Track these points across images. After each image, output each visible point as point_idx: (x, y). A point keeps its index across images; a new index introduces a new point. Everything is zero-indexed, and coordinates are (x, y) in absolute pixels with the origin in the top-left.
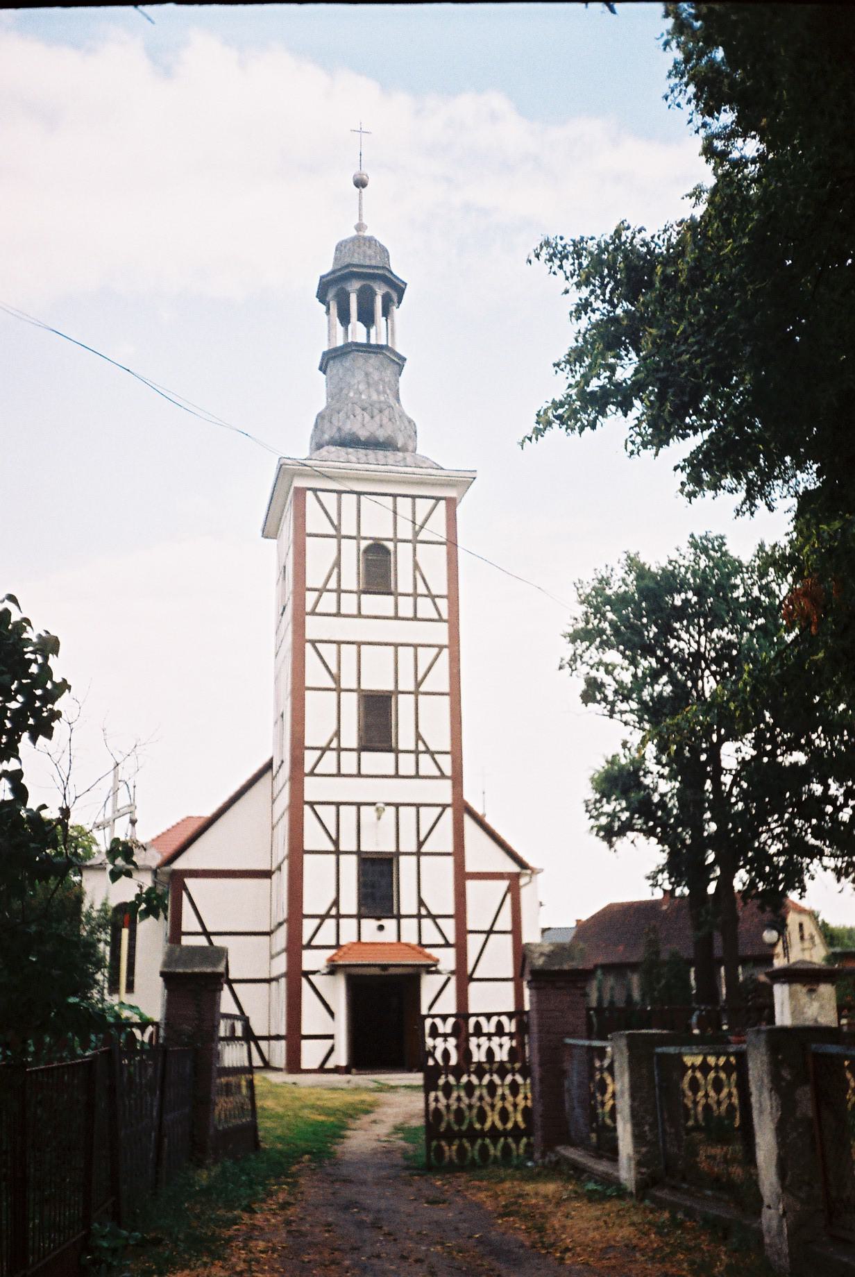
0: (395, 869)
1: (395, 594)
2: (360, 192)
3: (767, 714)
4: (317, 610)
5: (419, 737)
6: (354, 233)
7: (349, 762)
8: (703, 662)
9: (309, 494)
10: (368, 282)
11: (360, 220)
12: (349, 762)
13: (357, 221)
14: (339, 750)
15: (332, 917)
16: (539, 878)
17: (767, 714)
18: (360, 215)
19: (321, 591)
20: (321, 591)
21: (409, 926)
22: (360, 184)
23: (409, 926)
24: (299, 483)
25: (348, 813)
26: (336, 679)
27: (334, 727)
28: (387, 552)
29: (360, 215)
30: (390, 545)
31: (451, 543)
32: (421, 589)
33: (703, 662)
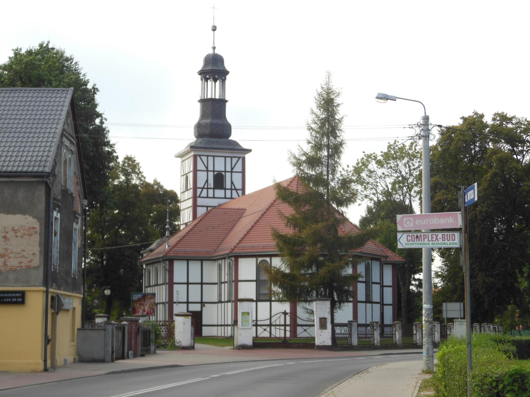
1: (225, 189)
2: (214, 48)
4: (201, 196)
5: (232, 183)
6: (211, 52)
7: (211, 194)
9: (198, 157)
11: (214, 44)
12: (211, 192)
13: (212, 45)
14: (208, 188)
15: (205, 188)
19: (203, 188)
20: (203, 188)
21: (228, 193)
22: (214, 29)
23: (228, 193)
25: (211, 159)
26: (207, 168)
27: (206, 178)
28: (222, 175)
30: (224, 173)
31: (243, 172)
32: (233, 188)
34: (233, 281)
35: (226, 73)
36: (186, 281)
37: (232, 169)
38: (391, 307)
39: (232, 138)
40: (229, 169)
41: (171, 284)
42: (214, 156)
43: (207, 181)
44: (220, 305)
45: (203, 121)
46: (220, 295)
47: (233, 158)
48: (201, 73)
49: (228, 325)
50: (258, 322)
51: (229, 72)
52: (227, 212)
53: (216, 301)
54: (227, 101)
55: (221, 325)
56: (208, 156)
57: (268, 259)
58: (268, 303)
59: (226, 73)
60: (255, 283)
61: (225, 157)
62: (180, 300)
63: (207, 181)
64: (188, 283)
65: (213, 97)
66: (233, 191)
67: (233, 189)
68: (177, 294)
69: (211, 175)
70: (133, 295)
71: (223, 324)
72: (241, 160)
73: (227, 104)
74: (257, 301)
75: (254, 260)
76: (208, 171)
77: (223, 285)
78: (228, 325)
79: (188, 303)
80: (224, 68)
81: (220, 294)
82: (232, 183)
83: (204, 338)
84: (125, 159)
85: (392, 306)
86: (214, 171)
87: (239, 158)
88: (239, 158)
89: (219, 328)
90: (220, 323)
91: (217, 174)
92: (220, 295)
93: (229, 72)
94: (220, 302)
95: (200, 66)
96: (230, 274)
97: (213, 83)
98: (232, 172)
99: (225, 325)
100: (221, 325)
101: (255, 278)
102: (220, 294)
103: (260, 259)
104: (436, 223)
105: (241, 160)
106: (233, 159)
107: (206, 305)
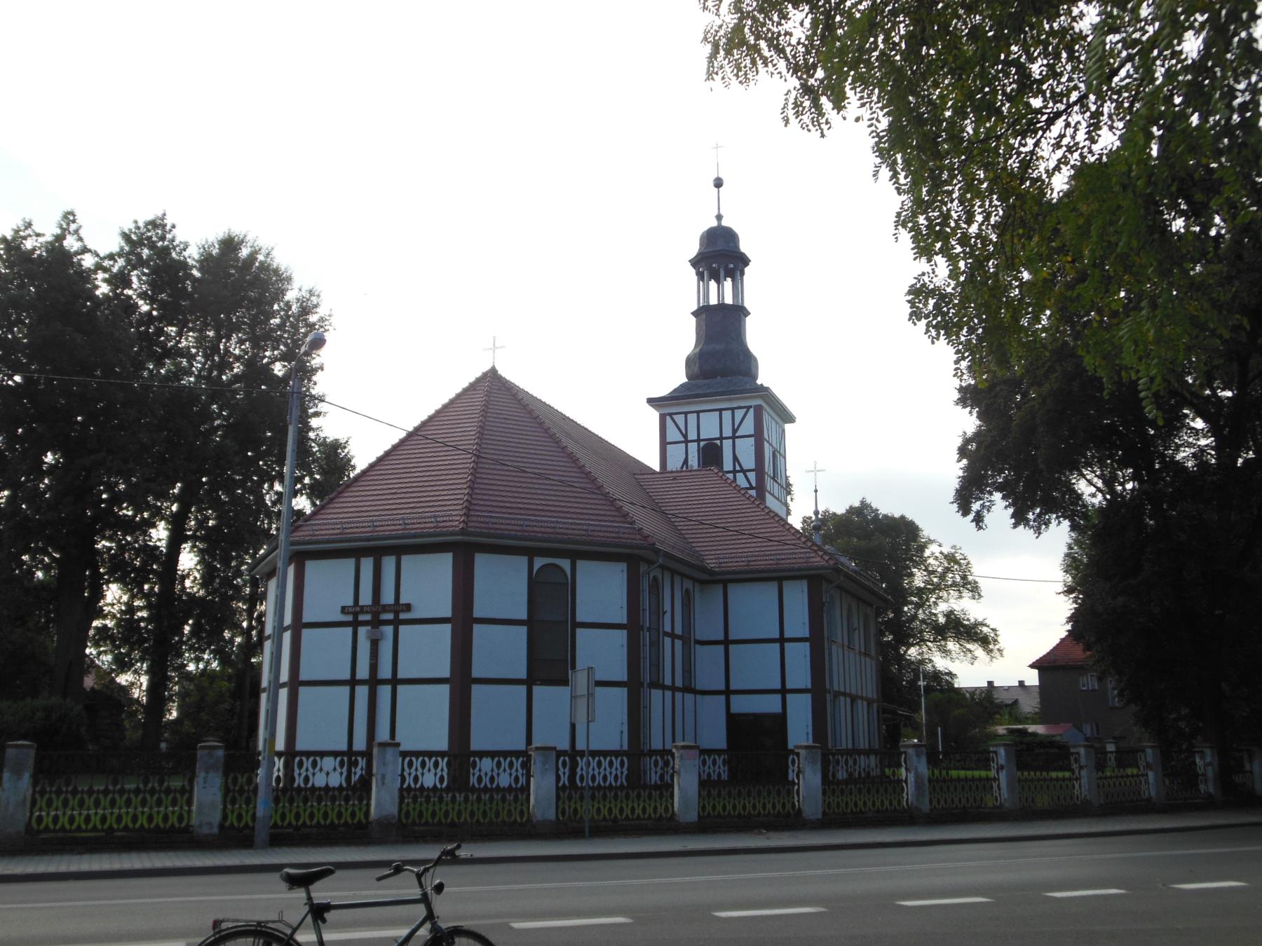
2: (719, 217)
5: (735, 459)
6: (714, 223)
9: (668, 417)
13: (716, 213)
22: (718, 183)
25: (692, 418)
26: (685, 436)
29: (719, 208)
32: (738, 468)
35: (744, 261)
37: (735, 431)
38: (448, 627)
40: (727, 432)
41: (819, 690)
42: (698, 412)
43: (686, 461)
48: (695, 263)
56: (686, 413)
57: (565, 564)
59: (744, 261)
60: (523, 630)
61: (720, 410)
63: (686, 461)
66: (737, 474)
67: (738, 471)
69: (693, 447)
73: (749, 321)
74: (530, 682)
75: (523, 561)
76: (686, 442)
79: (728, 692)
80: (738, 248)
82: (735, 459)
85: (809, 696)
86: (698, 440)
88: (748, 408)
91: (705, 446)
95: (694, 249)
98: (734, 438)
101: (523, 615)
103: (539, 562)
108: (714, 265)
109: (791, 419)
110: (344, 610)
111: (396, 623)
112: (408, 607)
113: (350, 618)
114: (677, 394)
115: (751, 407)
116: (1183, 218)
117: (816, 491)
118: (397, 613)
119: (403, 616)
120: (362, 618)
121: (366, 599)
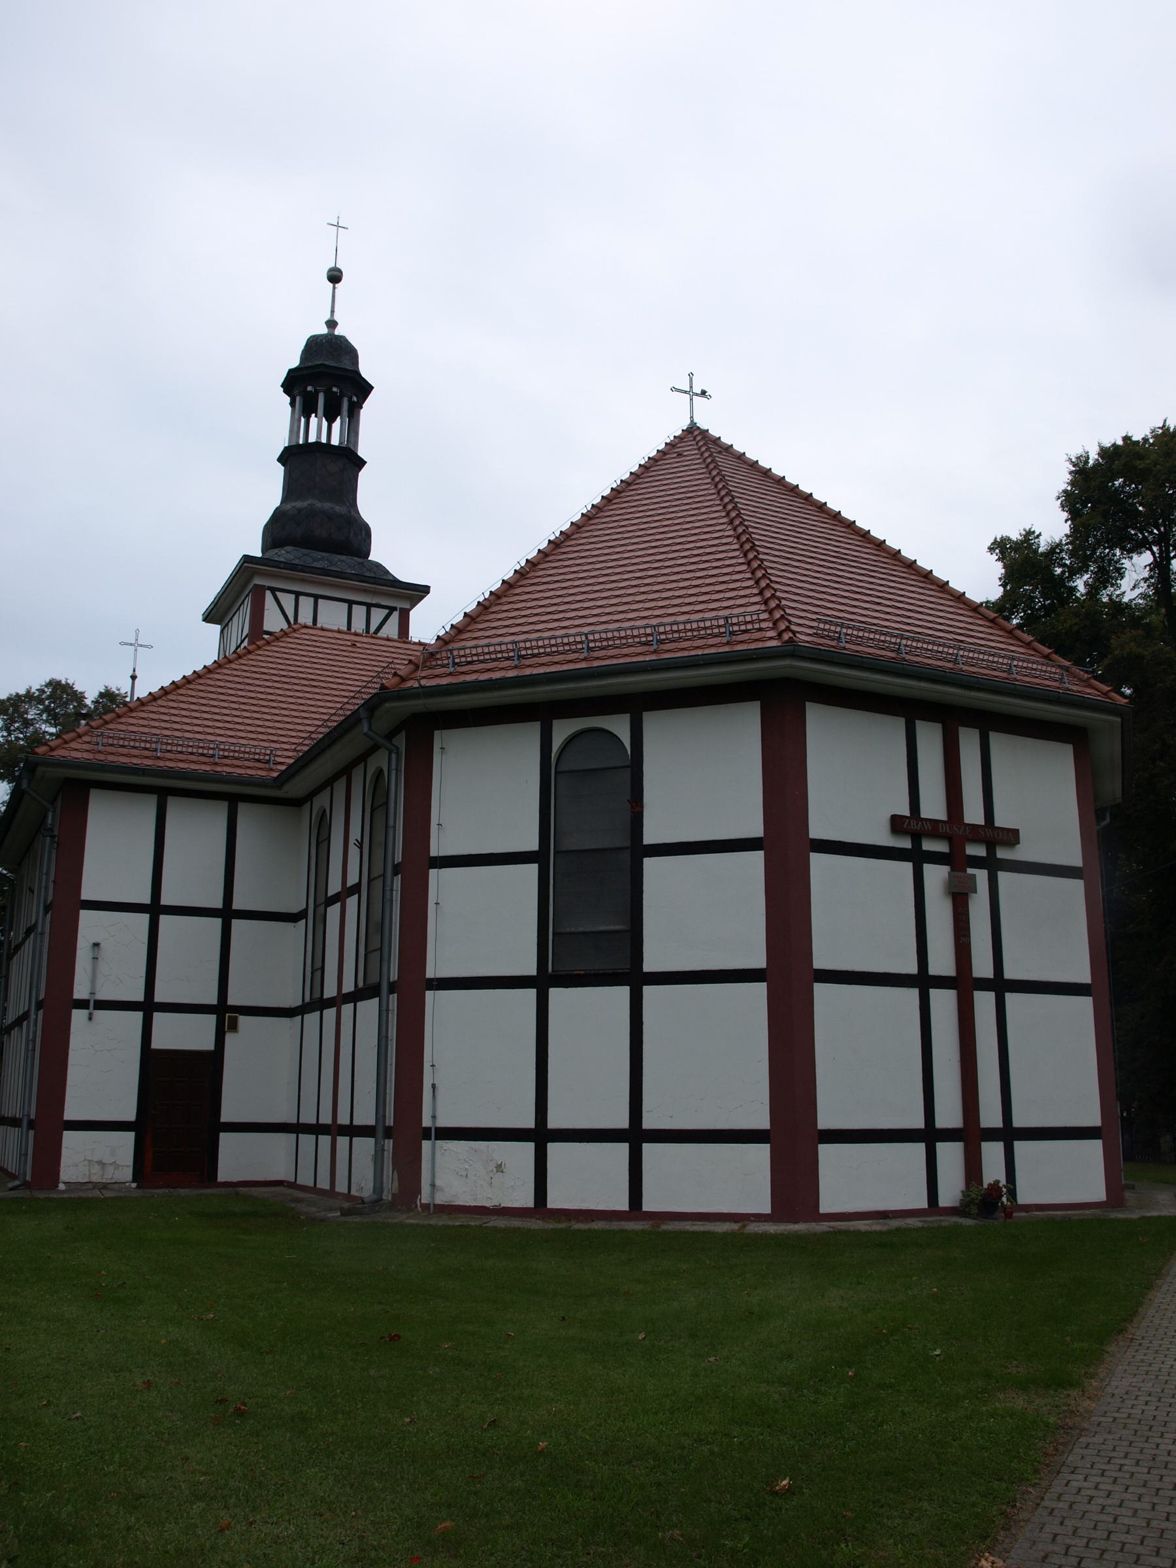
0: (688, 1226)
3: (1049, 602)
6: (324, 330)
8: (1157, 533)
9: (268, 594)
10: (251, 586)
13: (328, 317)
16: (107, 685)
17: (1049, 602)
18: (333, 312)
22: (335, 277)
24: (258, 581)
25: (306, 604)
29: (333, 312)
33: (1157, 533)
34: (397, 870)
36: (144, 896)
39: (373, 557)
44: (312, 1018)
45: (288, 506)
46: (316, 970)
47: (372, 609)
49: (353, 1131)
50: (941, 1122)
51: (365, 462)
52: (357, 644)
53: (294, 1001)
54: (361, 463)
55: (317, 1129)
57: (620, 726)
58: (622, 994)
61: (351, 603)
62: (106, 993)
64: (155, 909)
65: (324, 440)
68: (95, 958)
70: (425, 1198)
71: (326, 1119)
72: (396, 615)
77: (334, 911)
78: (353, 1131)
79: (148, 1007)
81: (318, 964)
83: (223, 1190)
84: (101, 695)
87: (392, 609)
89: (307, 1140)
90: (308, 1118)
92: (316, 970)
93: (365, 462)
94: (318, 1004)
96: (374, 841)
97: (325, 424)
99: (335, 1130)
100: (317, 1129)
102: (318, 964)
103: (562, 731)
104: (912, 828)
105: (396, 615)
106: (374, 610)
107: (243, 1020)
108: (335, 389)
109: (84, 693)
110: (897, 824)
111: (993, 865)
112: (1012, 837)
113: (906, 843)
114: (737, 480)
115: (395, 609)
116: (1171, 430)
117: (134, 678)
118: (991, 847)
119: (1002, 854)
120: (928, 845)
121: (933, 807)
